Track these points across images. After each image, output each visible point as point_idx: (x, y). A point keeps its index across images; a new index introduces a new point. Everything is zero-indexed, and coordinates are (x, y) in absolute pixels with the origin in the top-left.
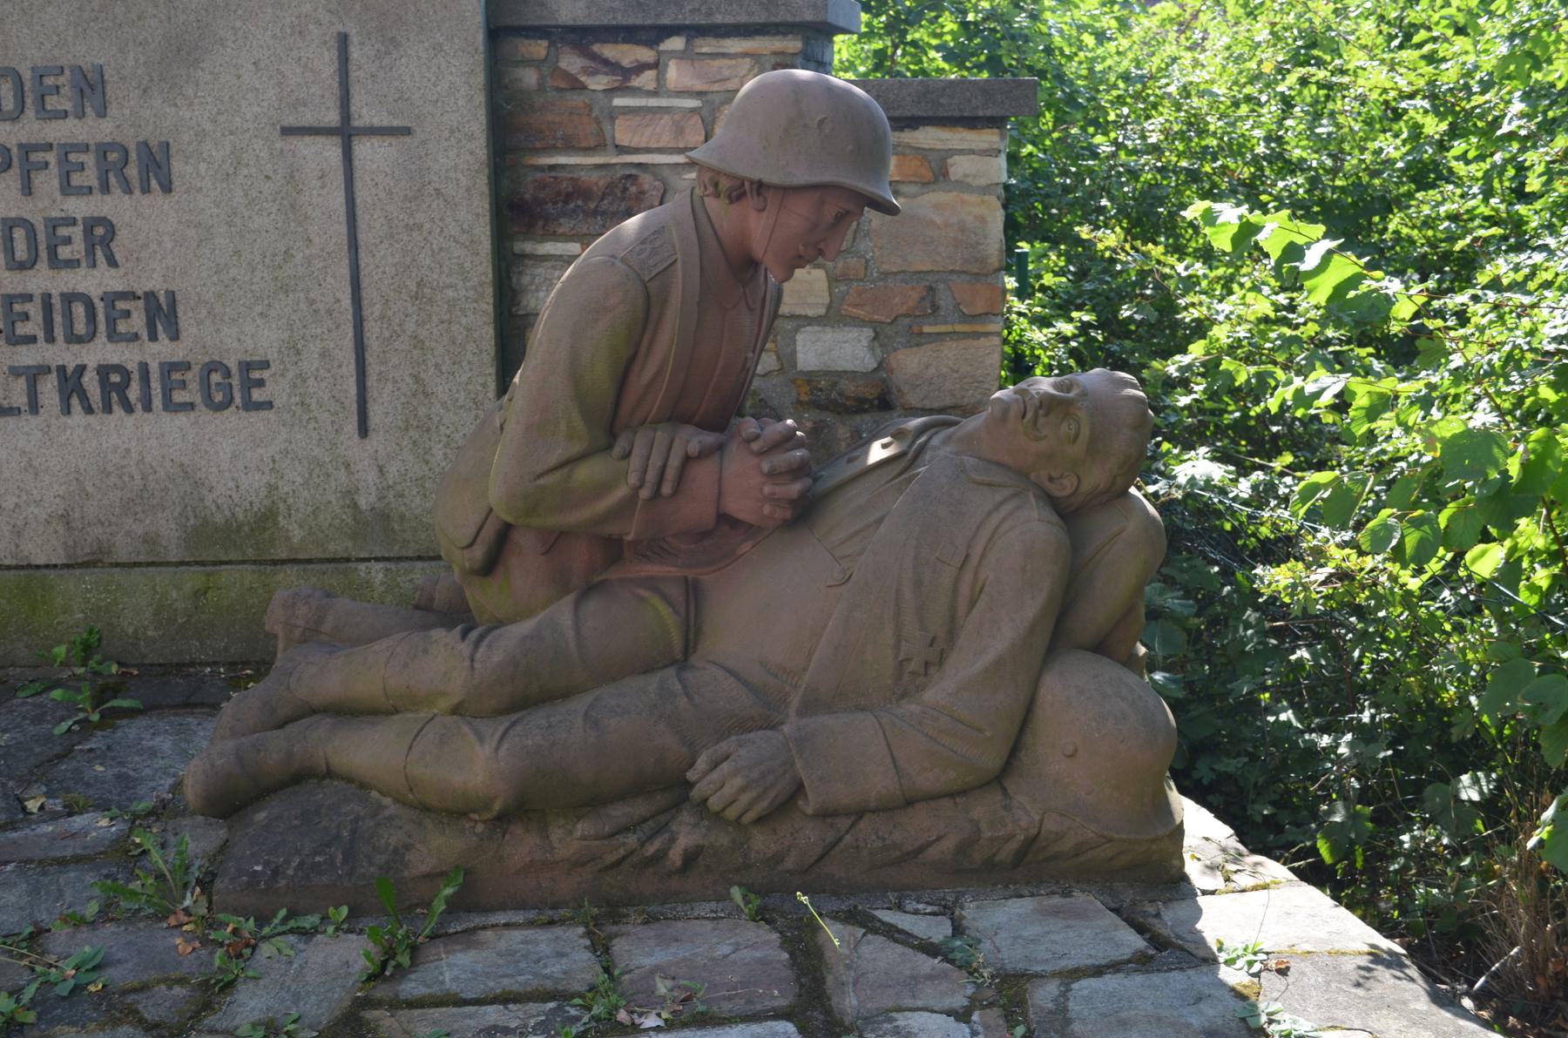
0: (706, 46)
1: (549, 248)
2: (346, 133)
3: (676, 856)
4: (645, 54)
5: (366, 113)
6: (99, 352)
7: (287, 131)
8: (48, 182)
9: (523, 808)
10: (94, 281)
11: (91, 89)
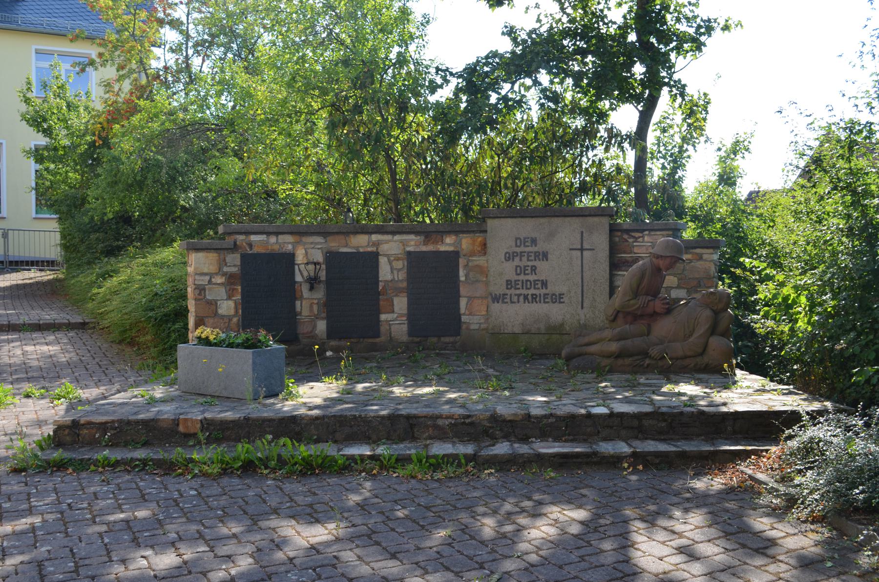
0: (653, 233)
1: (620, 273)
2: (582, 250)
3: (645, 365)
4: (640, 235)
5: (586, 246)
6: (532, 291)
7: (571, 249)
8: (525, 259)
9: (619, 355)
10: (532, 278)
11: (534, 241)
